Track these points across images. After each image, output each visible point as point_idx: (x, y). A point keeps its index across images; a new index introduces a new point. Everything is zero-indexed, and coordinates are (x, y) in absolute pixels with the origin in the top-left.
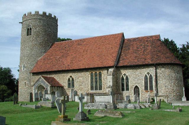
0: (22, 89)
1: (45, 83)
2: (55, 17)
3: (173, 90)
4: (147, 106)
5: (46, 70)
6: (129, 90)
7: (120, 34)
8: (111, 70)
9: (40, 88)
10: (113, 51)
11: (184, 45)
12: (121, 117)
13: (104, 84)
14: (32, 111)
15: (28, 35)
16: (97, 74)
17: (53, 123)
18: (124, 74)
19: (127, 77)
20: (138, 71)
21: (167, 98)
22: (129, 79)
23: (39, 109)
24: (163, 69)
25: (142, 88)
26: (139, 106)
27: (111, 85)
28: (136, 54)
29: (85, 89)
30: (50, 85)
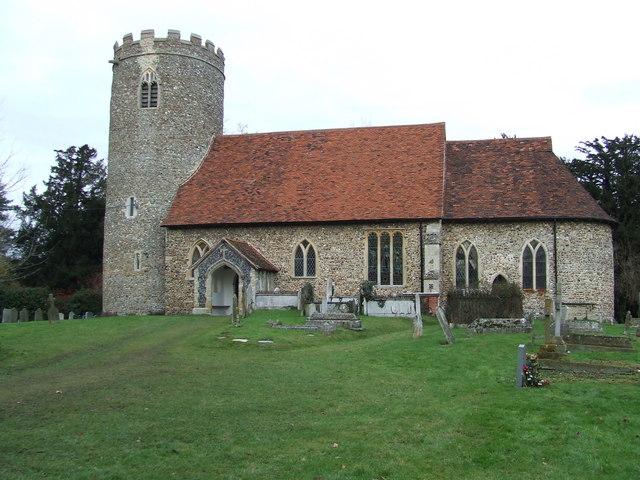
2: (196, 39)
20: (506, 235)
29: (349, 280)
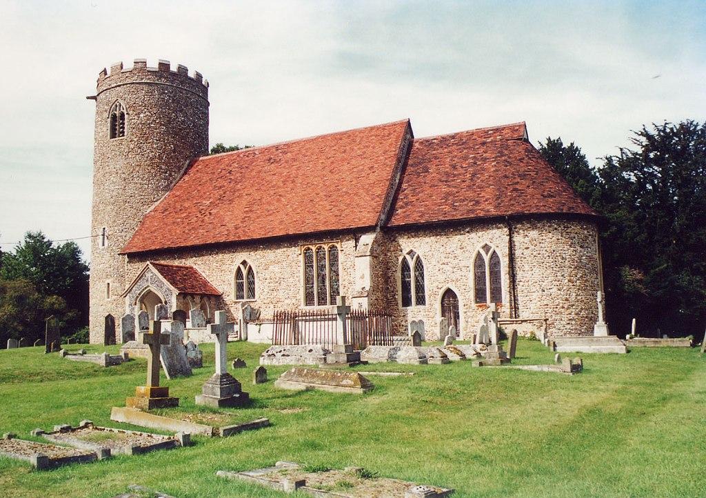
0: (100, 304)
1: (160, 286)
2: (199, 76)
3: (567, 300)
4: (470, 354)
5: (168, 244)
6: (424, 304)
7: (401, 124)
8: (367, 239)
9: (148, 299)
10: (373, 177)
11: (609, 160)
12: (359, 391)
13: (346, 283)
14: (94, 372)
15: (113, 135)
16: (324, 254)
17: (115, 414)
18: (408, 250)
19: (419, 265)
20: (455, 241)
21: (544, 326)
22: (425, 268)
23: (118, 368)
24: (534, 234)
25: (465, 296)
26: (438, 355)
27: (367, 288)
28: (449, 186)
30: (177, 292)
